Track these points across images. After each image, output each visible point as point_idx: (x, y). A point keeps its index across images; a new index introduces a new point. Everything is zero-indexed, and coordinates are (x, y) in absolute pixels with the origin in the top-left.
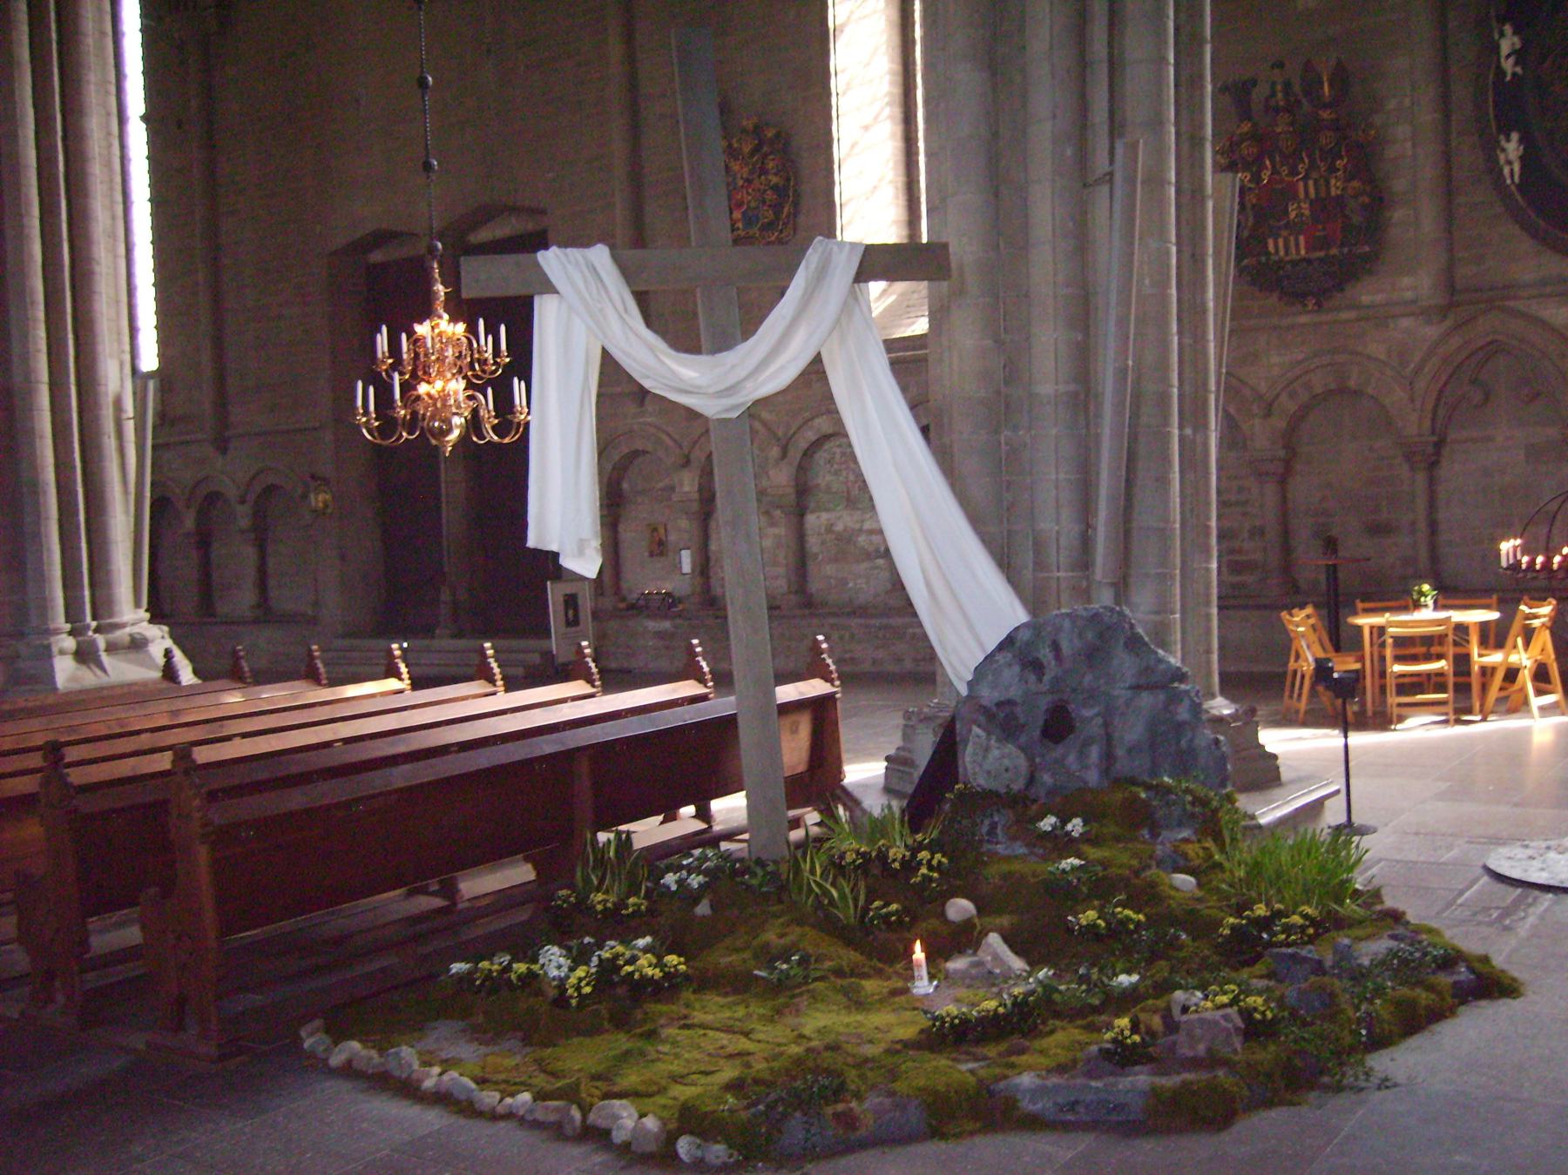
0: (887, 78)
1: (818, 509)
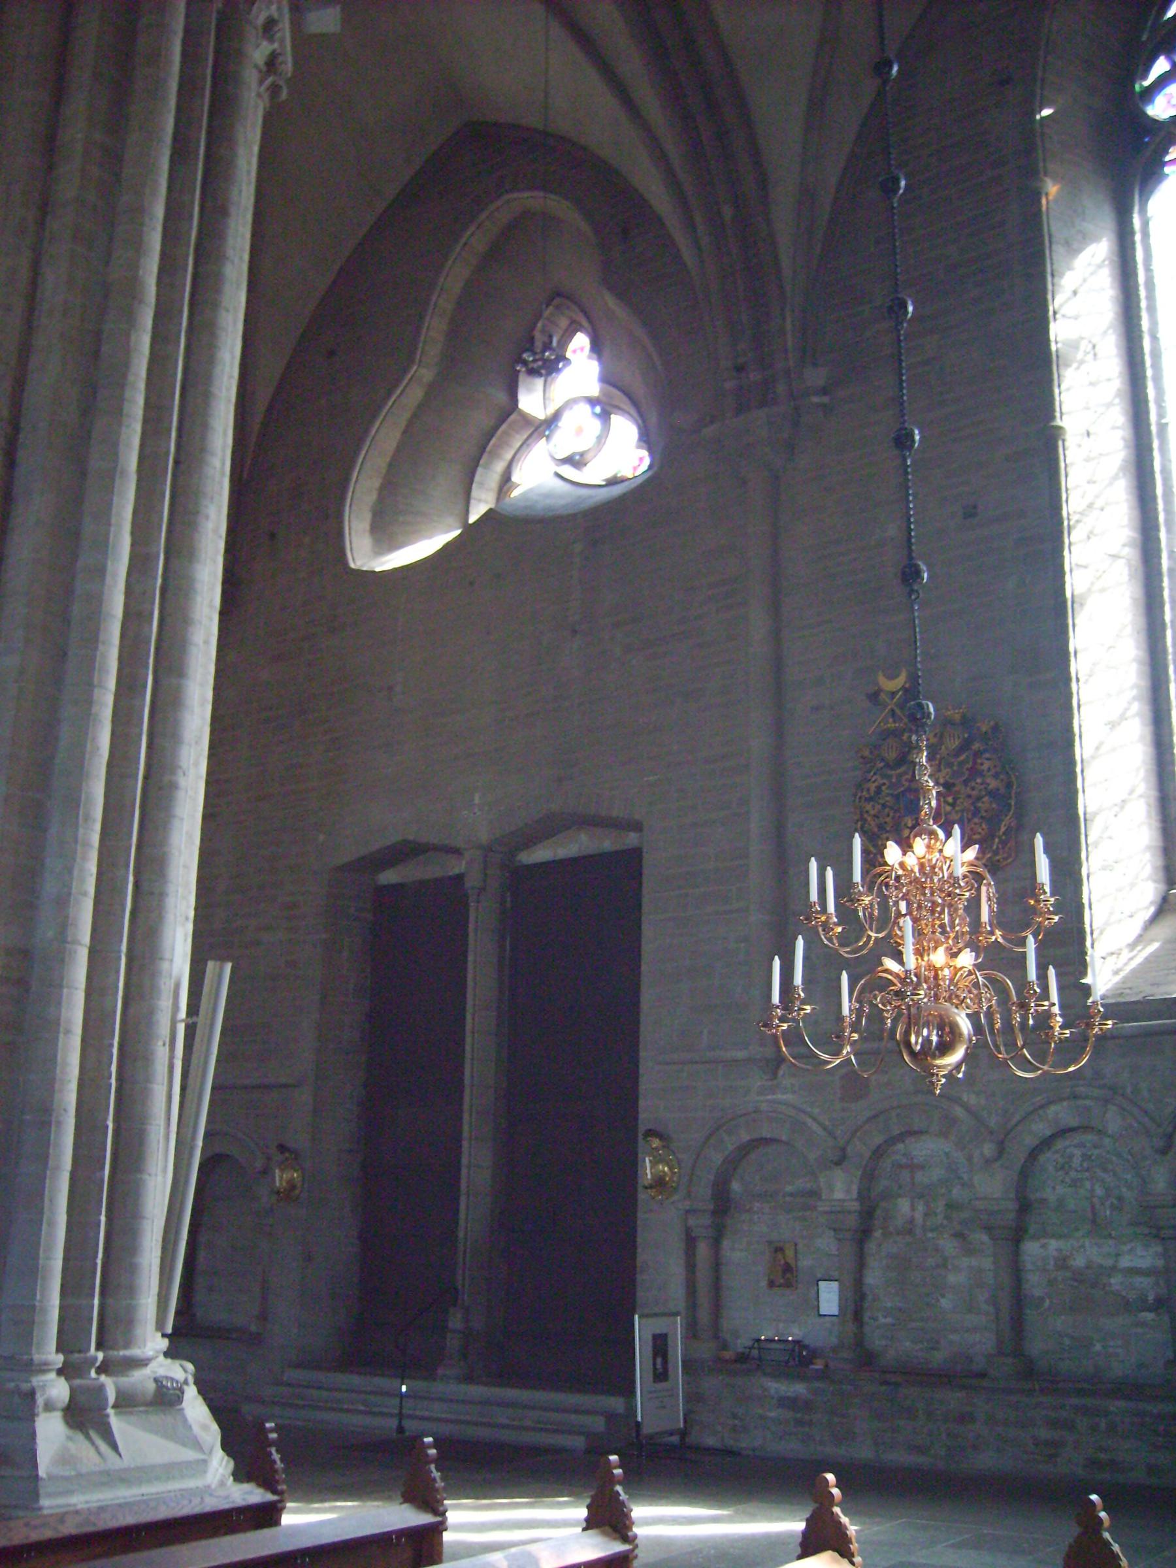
0: (1134, 667)
1: (1044, 1234)
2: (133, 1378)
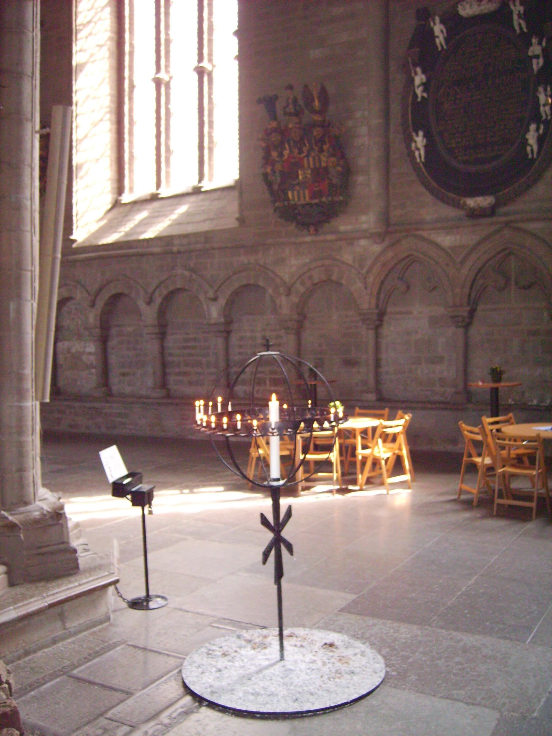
2: (475, 500)
